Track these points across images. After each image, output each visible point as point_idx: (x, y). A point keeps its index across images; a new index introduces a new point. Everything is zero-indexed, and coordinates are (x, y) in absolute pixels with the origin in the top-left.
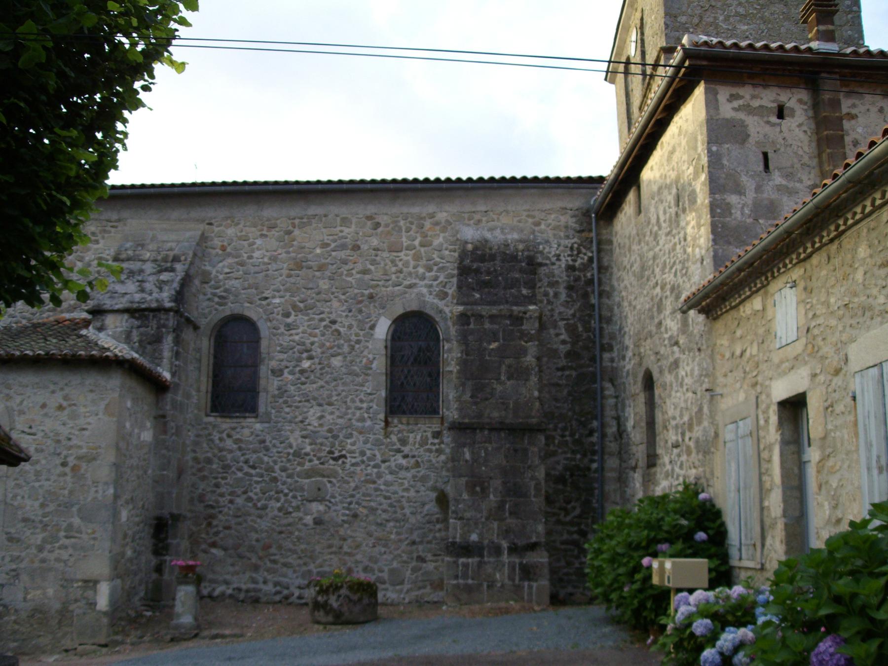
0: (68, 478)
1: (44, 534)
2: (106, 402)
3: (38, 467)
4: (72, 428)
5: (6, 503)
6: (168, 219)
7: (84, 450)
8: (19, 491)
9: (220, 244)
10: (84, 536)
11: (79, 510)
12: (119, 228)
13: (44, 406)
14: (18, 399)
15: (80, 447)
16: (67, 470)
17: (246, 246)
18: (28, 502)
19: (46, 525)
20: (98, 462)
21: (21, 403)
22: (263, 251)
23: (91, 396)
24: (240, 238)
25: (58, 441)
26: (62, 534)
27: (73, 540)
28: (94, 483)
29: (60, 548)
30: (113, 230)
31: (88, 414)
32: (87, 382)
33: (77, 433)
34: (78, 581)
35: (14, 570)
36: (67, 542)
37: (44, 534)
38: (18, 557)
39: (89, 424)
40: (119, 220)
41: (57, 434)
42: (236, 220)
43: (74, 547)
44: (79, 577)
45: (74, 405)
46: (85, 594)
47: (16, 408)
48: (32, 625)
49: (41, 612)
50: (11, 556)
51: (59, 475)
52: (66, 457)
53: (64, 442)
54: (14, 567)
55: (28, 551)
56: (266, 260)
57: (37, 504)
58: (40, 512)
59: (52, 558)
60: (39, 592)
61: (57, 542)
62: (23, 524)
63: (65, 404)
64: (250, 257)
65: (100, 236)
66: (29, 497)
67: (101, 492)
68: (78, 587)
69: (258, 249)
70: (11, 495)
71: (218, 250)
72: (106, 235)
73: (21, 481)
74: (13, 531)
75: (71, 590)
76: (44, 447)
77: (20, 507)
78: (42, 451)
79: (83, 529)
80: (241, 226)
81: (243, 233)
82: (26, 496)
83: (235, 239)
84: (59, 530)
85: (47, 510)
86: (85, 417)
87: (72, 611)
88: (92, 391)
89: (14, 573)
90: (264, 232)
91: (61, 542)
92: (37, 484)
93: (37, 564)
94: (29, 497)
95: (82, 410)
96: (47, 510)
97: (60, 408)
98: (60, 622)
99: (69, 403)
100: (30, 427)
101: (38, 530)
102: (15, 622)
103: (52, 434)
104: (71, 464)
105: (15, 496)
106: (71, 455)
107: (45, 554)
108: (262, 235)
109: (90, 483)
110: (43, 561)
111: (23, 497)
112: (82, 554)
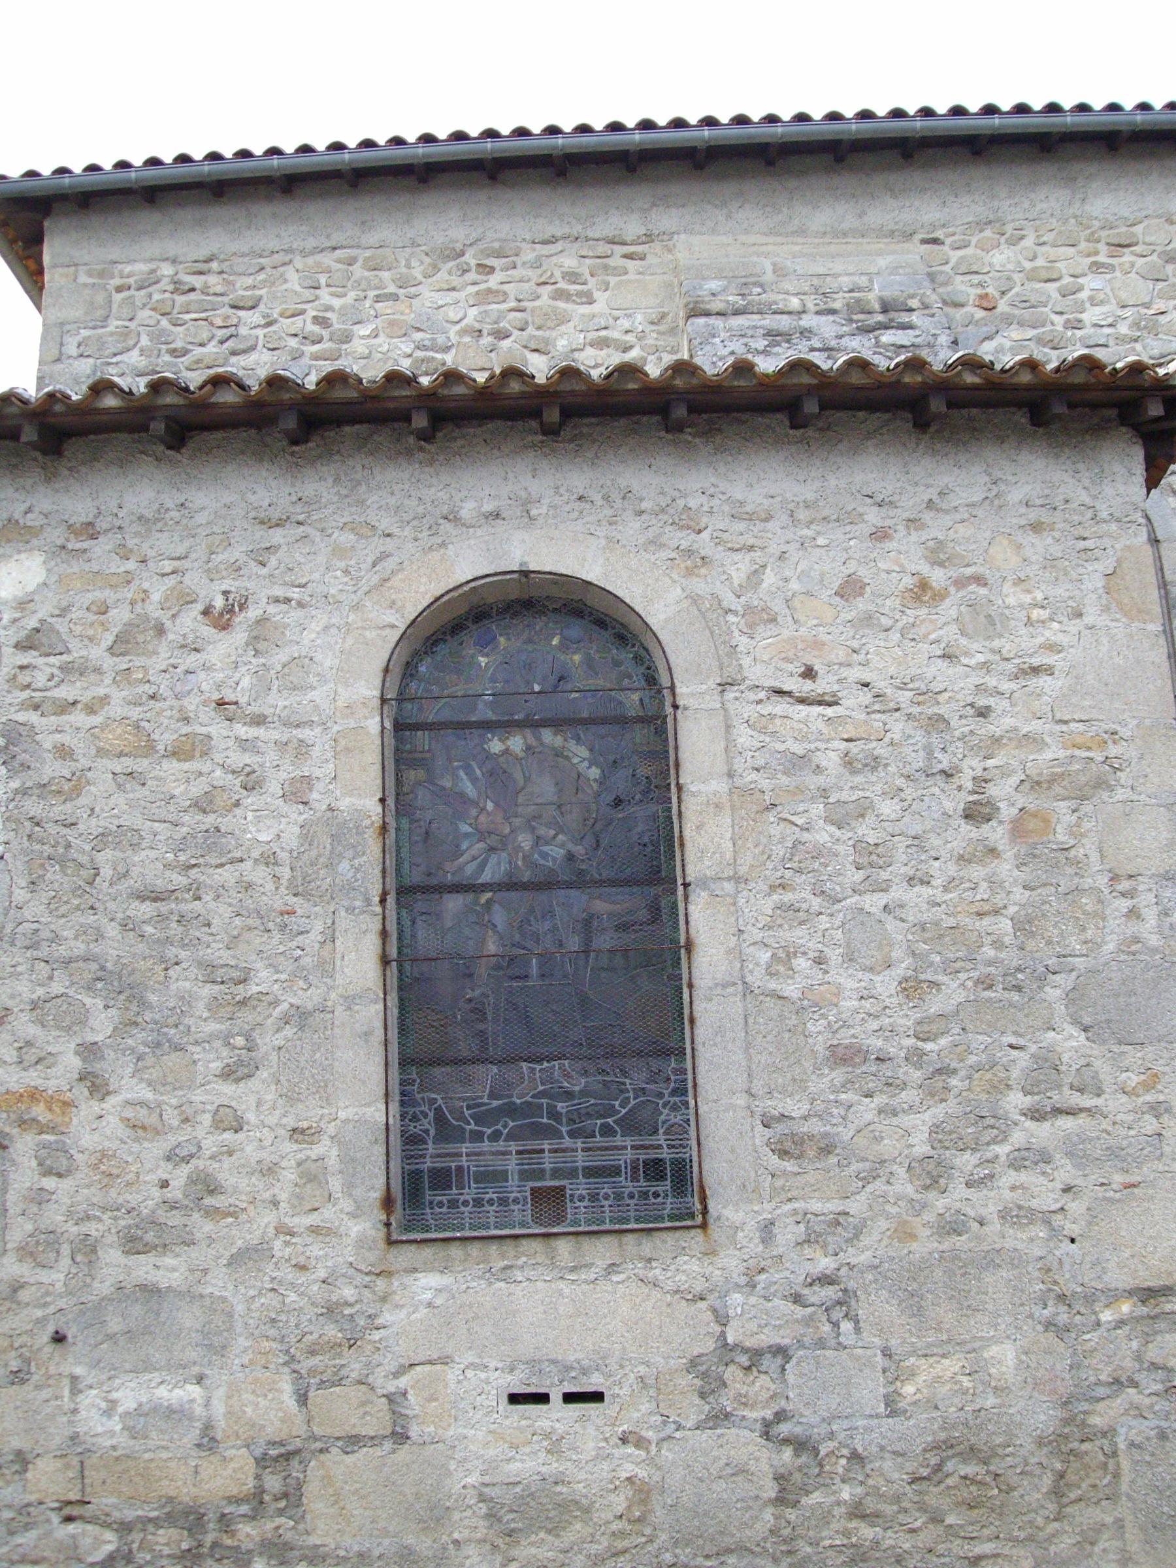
0: (1005, 868)
1: (937, 1112)
2: (1107, 565)
3: (867, 831)
4: (986, 666)
5: (748, 990)
6: (802, 232)
7: (1054, 752)
8: (798, 935)
9: (974, 292)
10: (1114, 1103)
11: (1073, 997)
12: (650, 260)
13: (851, 588)
14: (739, 568)
15: (1033, 741)
16: (996, 833)
17: (1055, 295)
18: (848, 981)
19: (944, 1071)
20: (1120, 794)
21: (755, 576)
22: (1111, 307)
23: (1037, 546)
24: (1032, 276)
25: (938, 723)
26: (1016, 1101)
27: (1067, 1123)
28: (1115, 878)
29: (1017, 1163)
30: (630, 265)
31: (1036, 614)
32: (1015, 495)
33: (1006, 686)
34: (1114, 1296)
35: (826, 1280)
36: (1043, 1133)
37: (937, 1112)
38: (837, 1221)
39: (1053, 648)
40: (649, 238)
41: (926, 695)
42: (1009, 229)
43: (1075, 1151)
44: (1118, 1278)
45: (980, 580)
46: (1153, 1353)
47: (729, 600)
48: (936, 1519)
49: (971, 1453)
50: (803, 1217)
51: (963, 859)
52: (981, 782)
53: (960, 727)
54: (825, 1264)
55: (879, 1186)
56: (1123, 329)
57: (886, 985)
58: (906, 1019)
59: (991, 1211)
60: (950, 1366)
61: (1003, 1138)
62: (838, 1075)
63: (938, 577)
64: (1077, 325)
65: (592, 283)
66: (850, 958)
67: (1151, 916)
68: (1120, 1323)
69: (1094, 302)
70: (765, 956)
71: (969, 309)
72: (613, 280)
73: (802, 895)
74: (795, 1107)
75: (1093, 1338)
76: (881, 750)
77: (808, 1005)
78: (874, 763)
79: (1103, 1069)
80: (1029, 242)
81: (1040, 262)
82: (834, 956)
83: (1017, 277)
84: (1001, 1087)
85: (936, 1004)
86: (1029, 622)
87: (1108, 1433)
88: (1037, 527)
89: (829, 1293)
90: (1101, 258)
91: (1017, 1138)
92: (873, 902)
93: (925, 1245)
94: (850, 958)
95: (1013, 597)
96: (936, 1004)
97: (922, 591)
98: (1057, 1493)
99: (954, 573)
100: (809, 673)
101: (908, 1096)
102: (858, 1512)
103: (905, 697)
104: (1007, 812)
105: (785, 958)
106: (1004, 771)
107: (956, 1196)
108: (1096, 267)
109: (1102, 881)
110: (952, 1226)
111: (820, 961)
112: (1118, 1178)
